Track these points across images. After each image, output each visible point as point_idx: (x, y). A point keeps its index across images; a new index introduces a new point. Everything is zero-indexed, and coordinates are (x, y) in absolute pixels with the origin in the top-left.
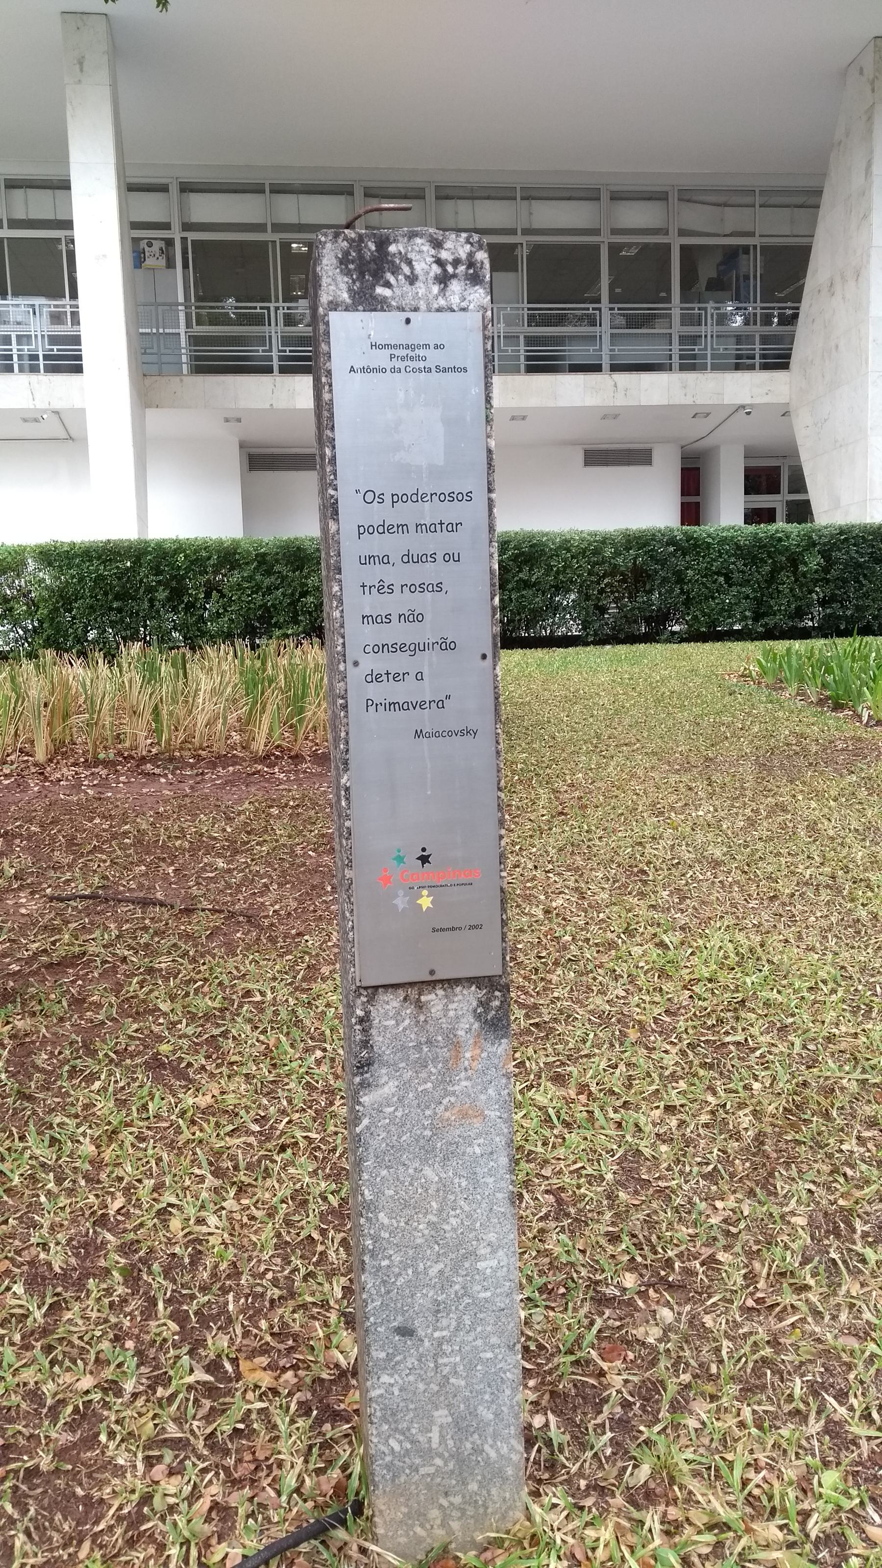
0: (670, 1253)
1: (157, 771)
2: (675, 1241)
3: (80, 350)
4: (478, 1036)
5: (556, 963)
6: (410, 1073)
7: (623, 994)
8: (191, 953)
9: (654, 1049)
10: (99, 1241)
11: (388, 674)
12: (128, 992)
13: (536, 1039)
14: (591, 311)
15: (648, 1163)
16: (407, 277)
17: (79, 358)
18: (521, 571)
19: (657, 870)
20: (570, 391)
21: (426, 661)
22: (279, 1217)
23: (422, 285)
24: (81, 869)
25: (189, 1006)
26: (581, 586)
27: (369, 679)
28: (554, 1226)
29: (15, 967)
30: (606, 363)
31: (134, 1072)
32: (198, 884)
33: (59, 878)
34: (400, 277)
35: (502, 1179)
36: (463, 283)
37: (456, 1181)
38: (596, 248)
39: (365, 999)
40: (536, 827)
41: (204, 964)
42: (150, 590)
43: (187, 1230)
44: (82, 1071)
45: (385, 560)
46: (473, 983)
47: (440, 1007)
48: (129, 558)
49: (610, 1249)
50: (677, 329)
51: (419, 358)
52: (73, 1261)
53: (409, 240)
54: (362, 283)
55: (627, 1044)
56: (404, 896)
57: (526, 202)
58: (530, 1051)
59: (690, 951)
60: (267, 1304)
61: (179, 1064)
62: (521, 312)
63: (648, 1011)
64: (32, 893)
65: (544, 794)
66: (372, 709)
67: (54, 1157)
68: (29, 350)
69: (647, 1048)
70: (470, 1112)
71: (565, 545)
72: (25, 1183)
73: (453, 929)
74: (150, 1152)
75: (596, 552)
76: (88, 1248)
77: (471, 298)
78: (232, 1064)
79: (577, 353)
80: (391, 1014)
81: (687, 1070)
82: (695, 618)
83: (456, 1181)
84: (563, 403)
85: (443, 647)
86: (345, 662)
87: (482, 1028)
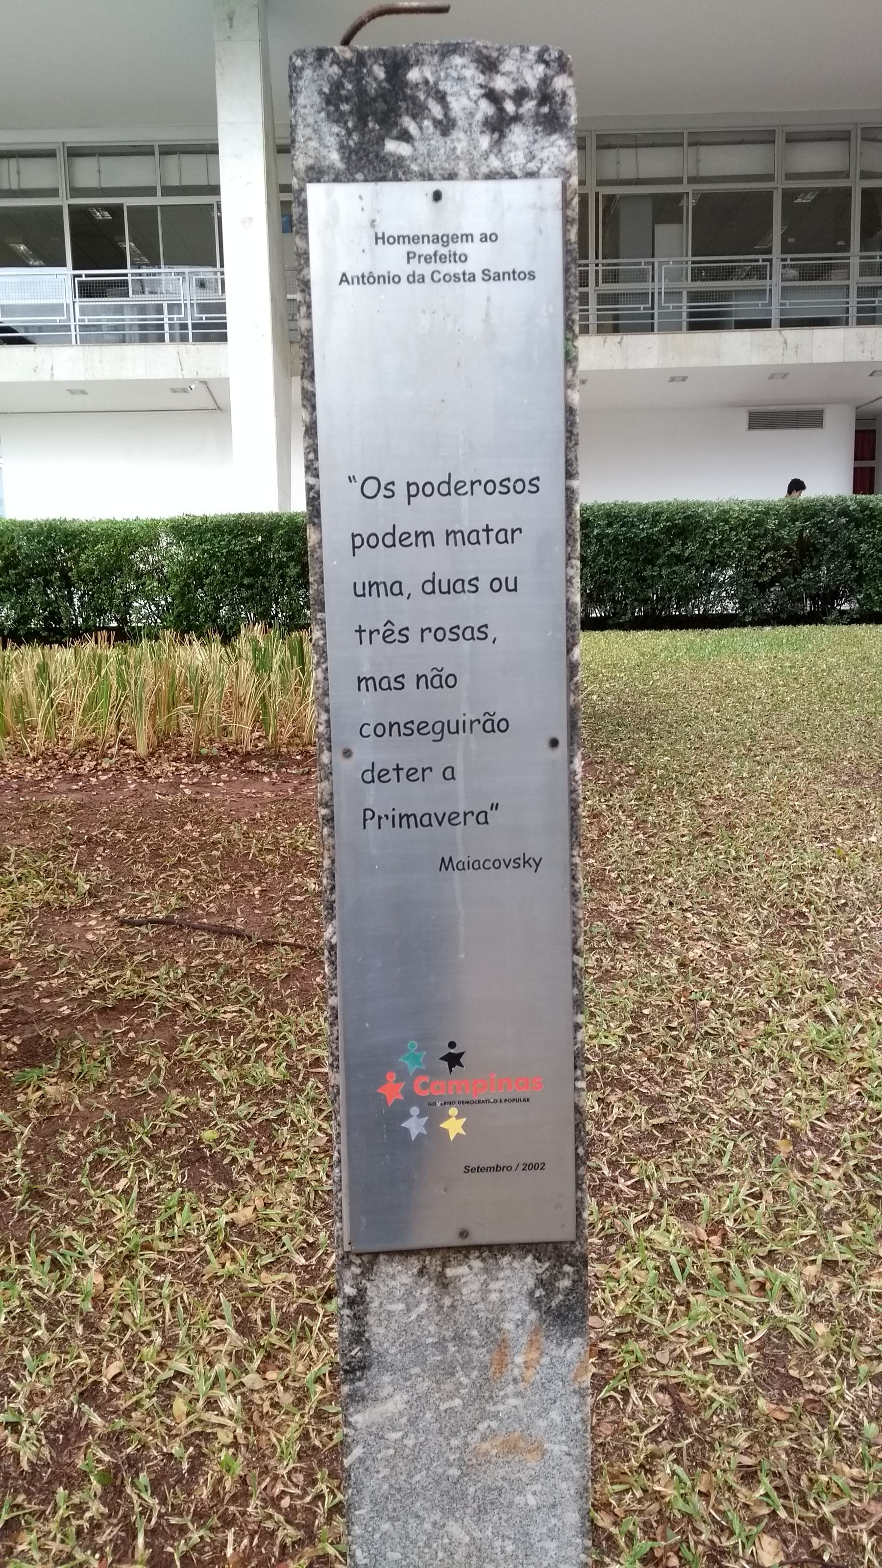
0: (826, 1510)
1: (261, 769)
2: (834, 1490)
3: (225, 318)
4: (536, 1332)
5: (690, 1037)
6: (427, 1383)
7: (772, 1085)
8: (260, 1003)
9: (811, 1170)
10: (83, 1424)
11: (398, 769)
12: (182, 1052)
13: (660, 1147)
14: (760, 263)
15: (799, 1351)
16: (437, 123)
17: (224, 326)
18: (673, 545)
19: (818, 913)
20: (736, 351)
21: (459, 750)
22: (310, 1407)
23: (462, 135)
24: (160, 886)
25: (245, 1077)
26: (739, 561)
27: (368, 777)
28: (669, 1448)
29: (65, 1010)
30: (775, 319)
31: (169, 1167)
32: (284, 909)
33: (136, 896)
34: (427, 123)
35: (569, 1544)
36: (531, 130)
37: (498, 1543)
38: (768, 195)
39: (358, 1271)
40: (675, 852)
41: (273, 1018)
42: (282, 566)
43: (192, 1418)
44: (109, 1162)
45: (395, 589)
46: (529, 1251)
47: (476, 1286)
48: (259, 532)
49: (743, 1492)
50: (855, 280)
51: (455, 257)
52: (46, 1452)
53: (441, 60)
54: (363, 135)
55: (776, 1161)
56: (420, 1116)
57: (694, 148)
58: (651, 1167)
59: (859, 1026)
60: (276, 1551)
61: (224, 1157)
62: (684, 266)
63: (804, 1113)
64: (104, 914)
65: (685, 808)
66: (372, 824)
67: (53, 1288)
68: (179, 319)
69: (802, 1170)
70: (522, 1444)
71: (724, 516)
72: (13, 1324)
73: (498, 1168)
74: (166, 1291)
75: (758, 524)
76: (66, 1433)
77: (544, 154)
78: (285, 1161)
79: (744, 308)
80: (398, 1294)
81: (853, 1205)
82: (868, 597)
83: (498, 1543)
84: (727, 362)
85: (488, 726)
86: (330, 749)
87: (541, 1320)
